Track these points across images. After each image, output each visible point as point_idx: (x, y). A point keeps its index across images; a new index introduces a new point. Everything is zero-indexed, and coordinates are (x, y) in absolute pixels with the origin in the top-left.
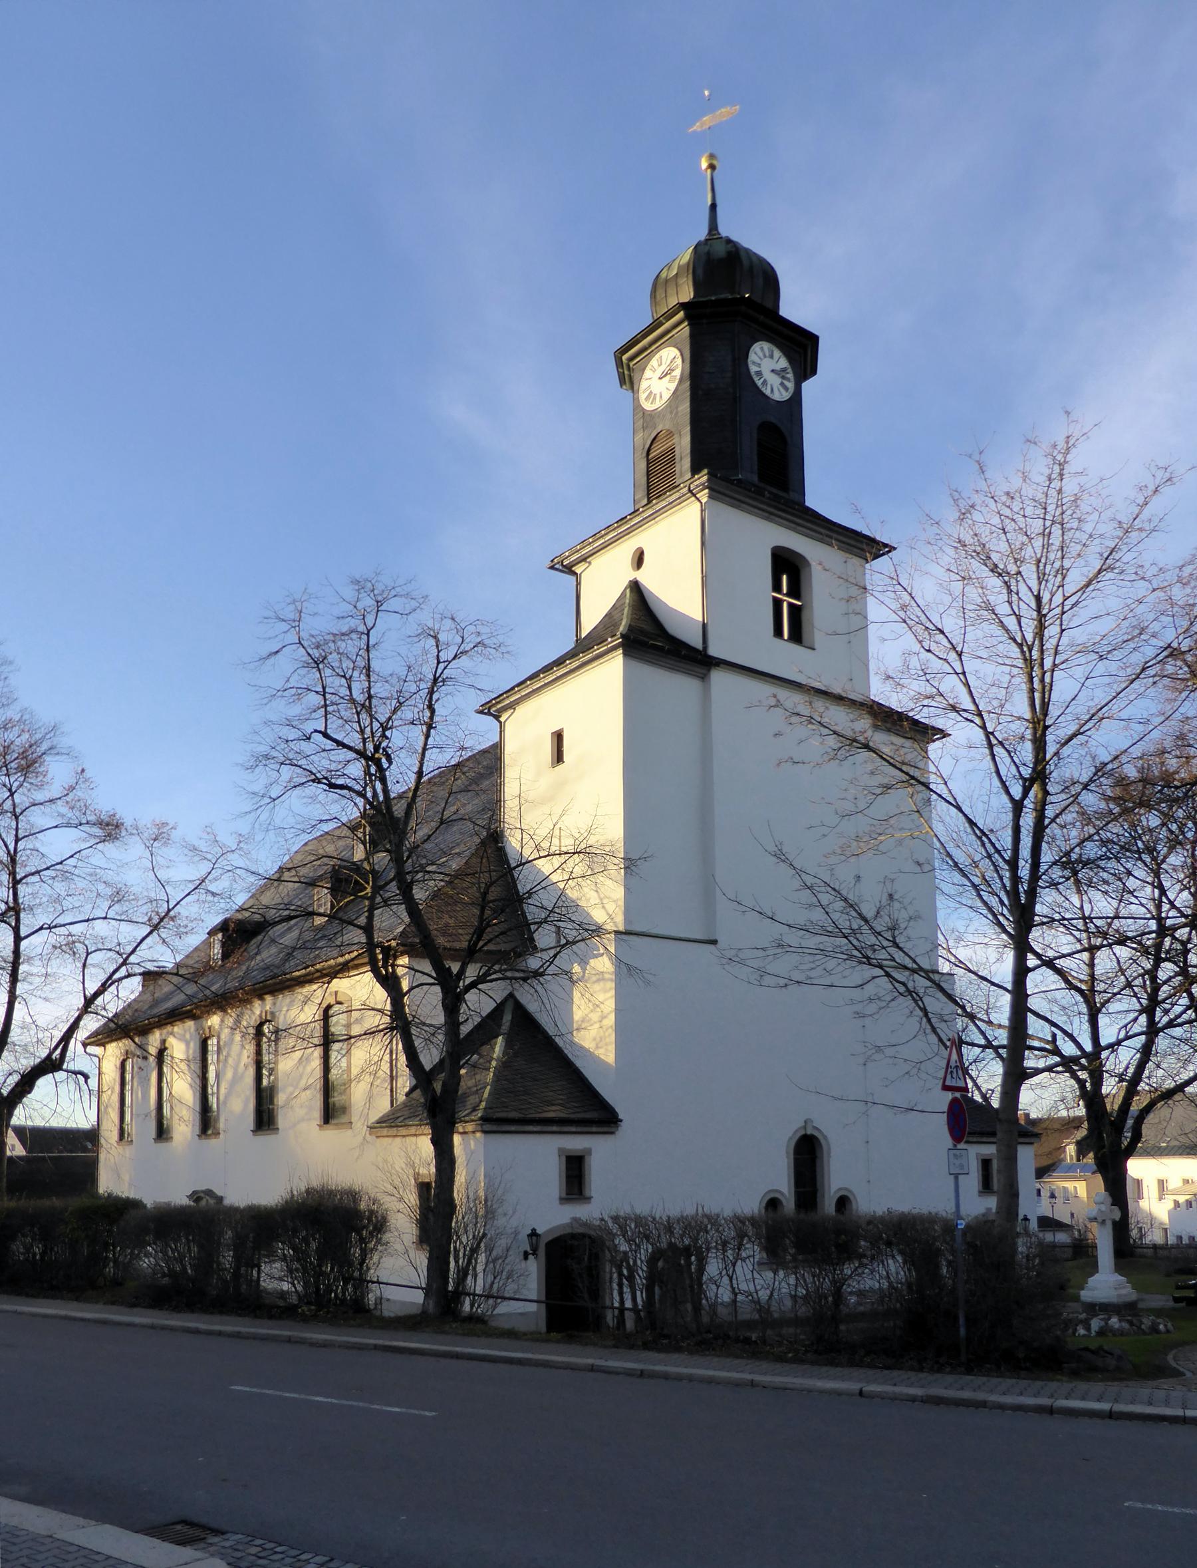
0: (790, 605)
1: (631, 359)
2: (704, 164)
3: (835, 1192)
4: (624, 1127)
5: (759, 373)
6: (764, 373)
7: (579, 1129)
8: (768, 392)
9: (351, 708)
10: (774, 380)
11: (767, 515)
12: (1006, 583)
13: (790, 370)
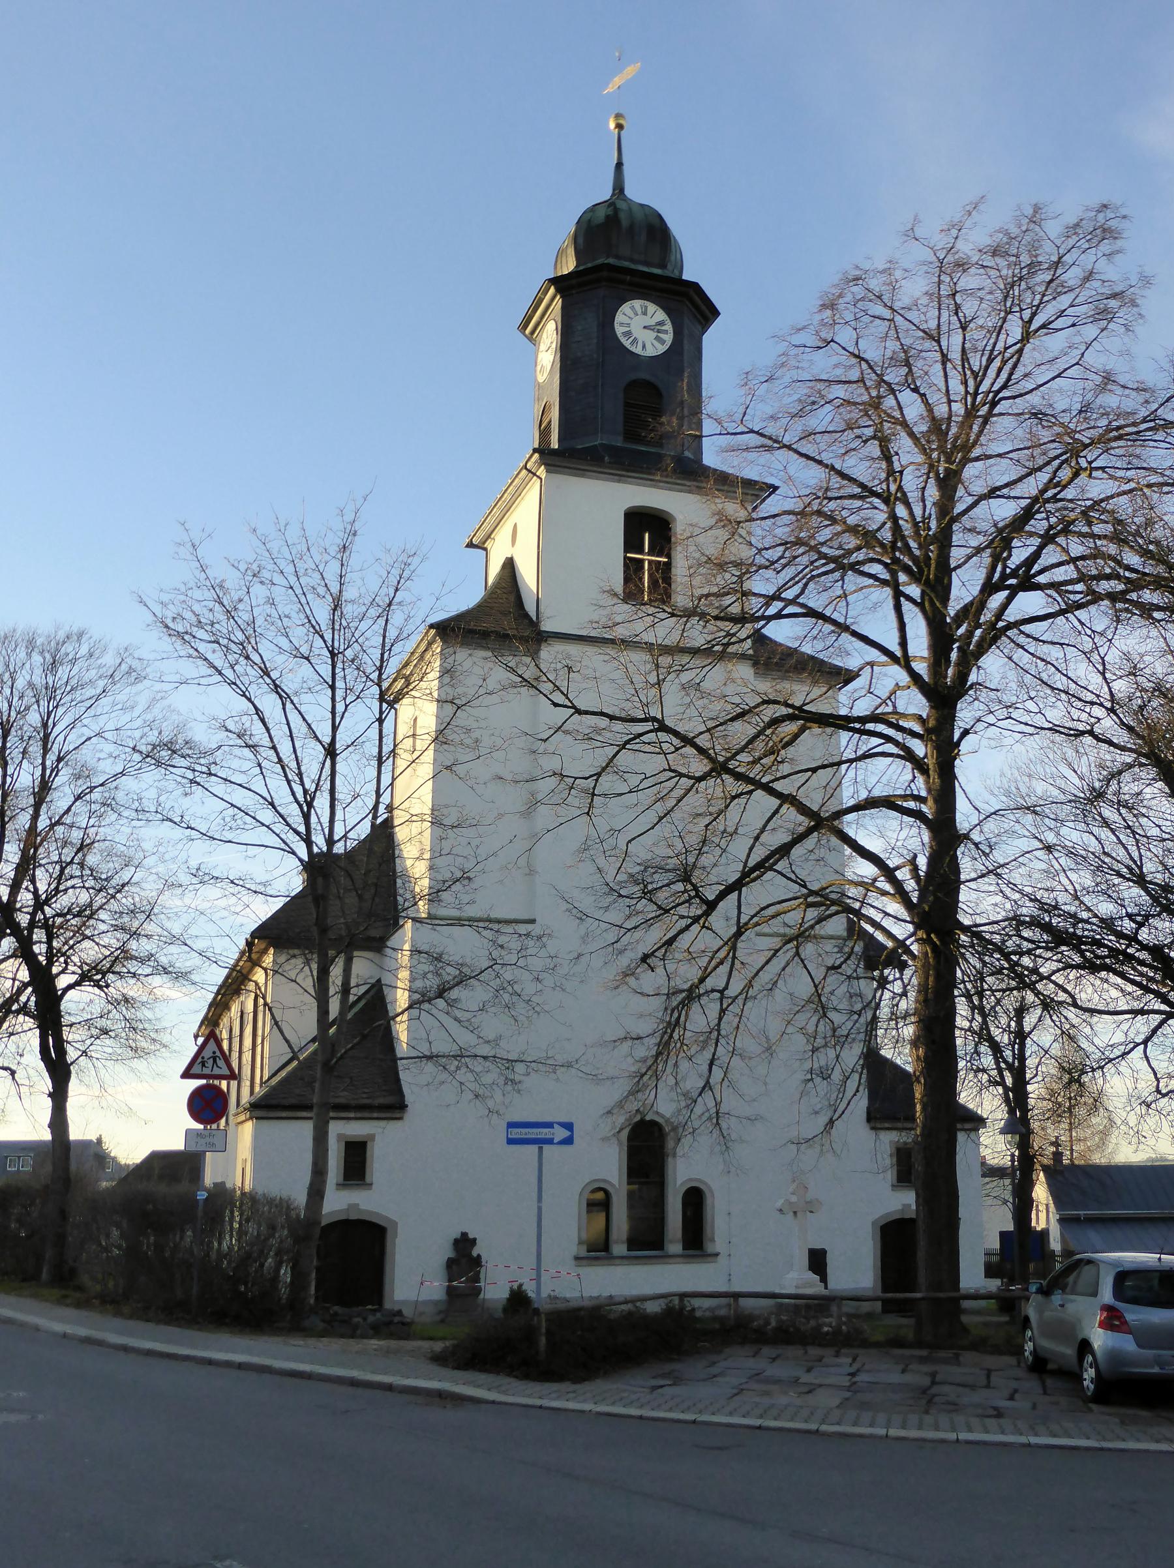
0: (650, 562)
1: (533, 332)
2: (612, 125)
3: (682, 1184)
4: (409, 1115)
5: (628, 334)
6: (633, 332)
7: (359, 1115)
8: (638, 350)
9: (716, 559)
10: (649, 336)
11: (616, 477)
12: (741, 564)
13: (668, 322)
